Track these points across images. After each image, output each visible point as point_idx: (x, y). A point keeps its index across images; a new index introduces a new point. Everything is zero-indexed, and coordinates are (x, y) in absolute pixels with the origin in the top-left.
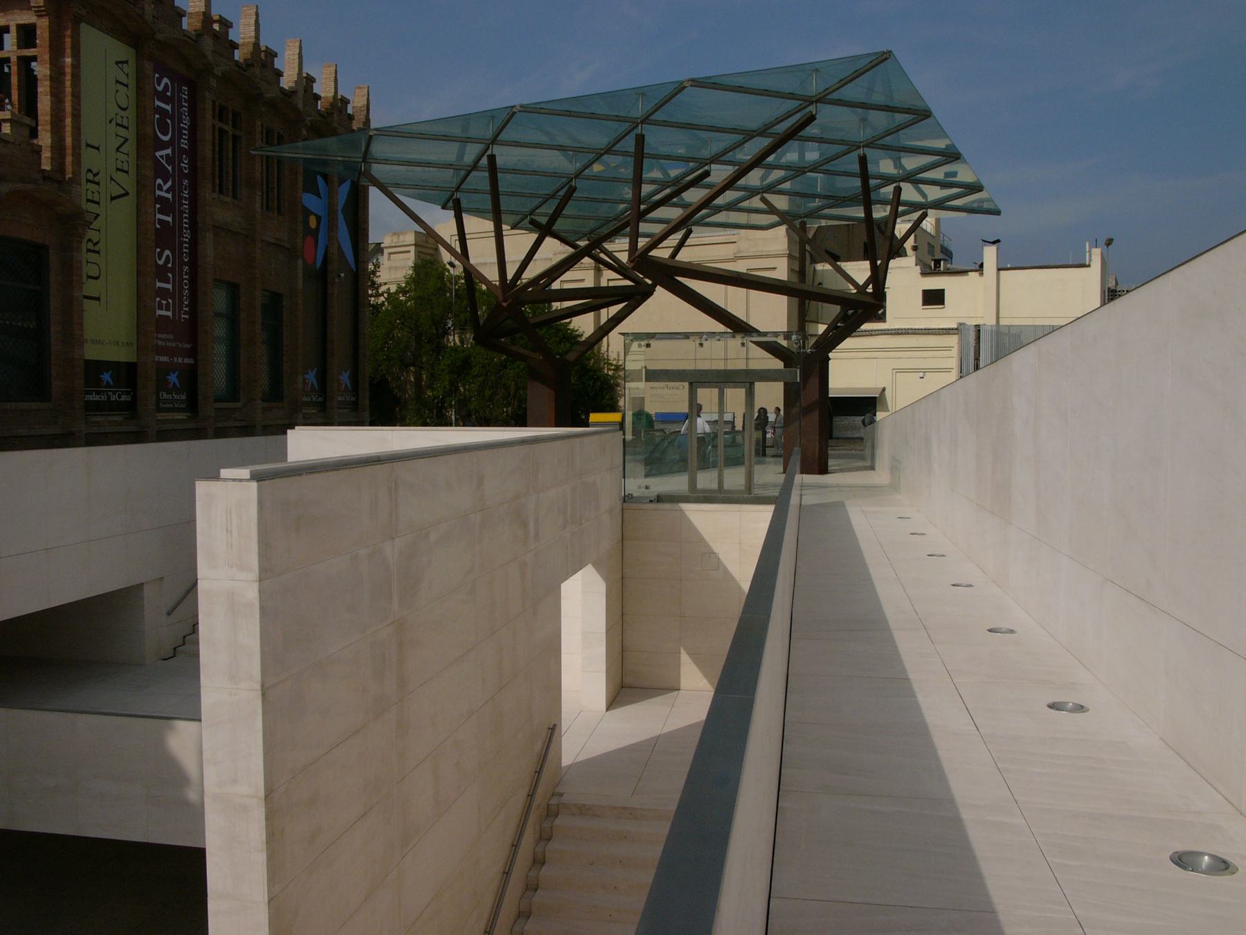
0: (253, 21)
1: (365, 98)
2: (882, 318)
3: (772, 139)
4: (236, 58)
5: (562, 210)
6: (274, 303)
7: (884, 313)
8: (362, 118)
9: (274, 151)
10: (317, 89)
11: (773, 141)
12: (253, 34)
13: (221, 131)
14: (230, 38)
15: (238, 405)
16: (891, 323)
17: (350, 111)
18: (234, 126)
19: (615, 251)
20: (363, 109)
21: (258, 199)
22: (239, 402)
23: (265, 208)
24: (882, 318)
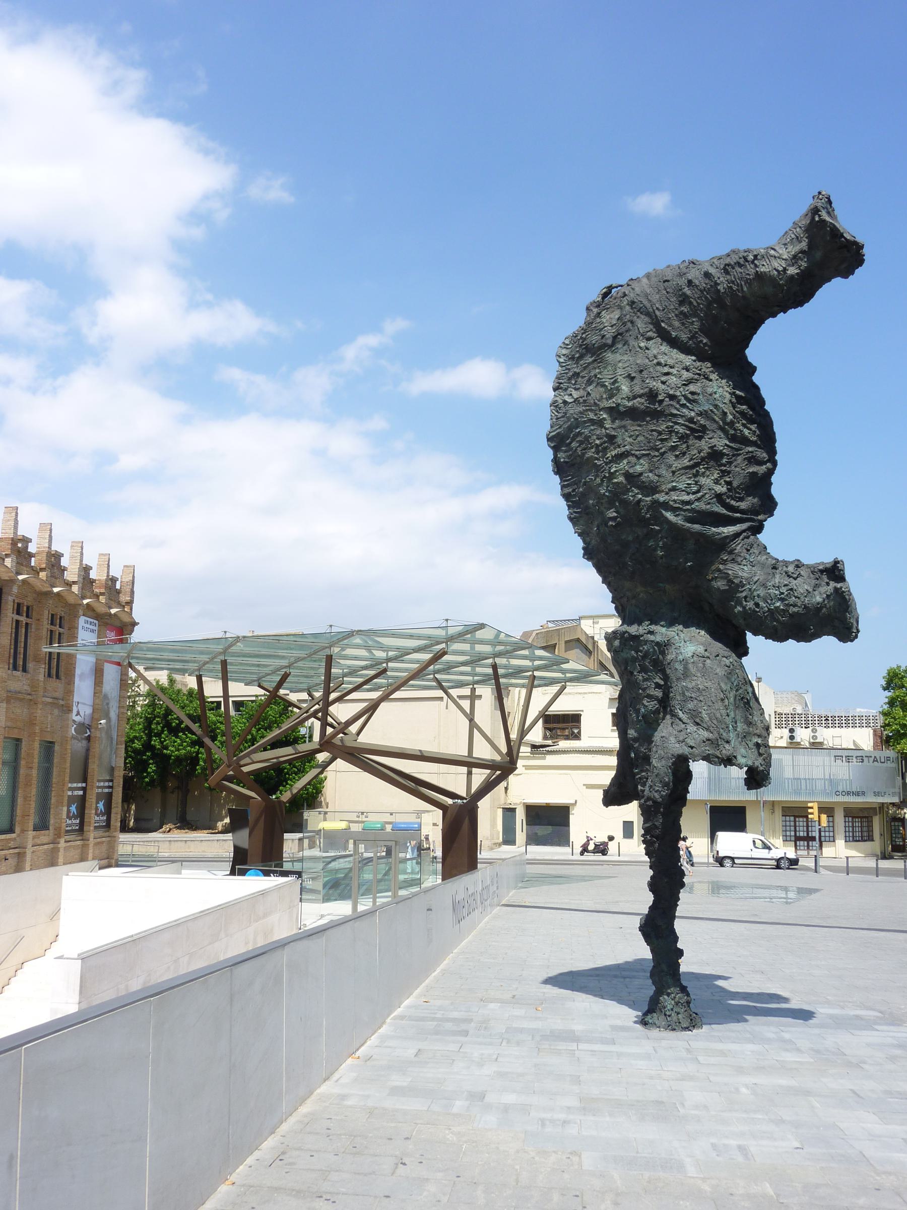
0: (47, 536)
1: (131, 575)
2: (577, 737)
3: (541, 719)
4: (33, 564)
5: (286, 679)
6: (48, 748)
7: (579, 733)
8: (128, 589)
9: (55, 648)
10: (93, 575)
11: (543, 720)
12: (47, 545)
13: (17, 622)
14: (29, 551)
15: (13, 836)
16: (584, 742)
17: (118, 587)
18: (27, 616)
19: (330, 716)
20: (129, 584)
21: (42, 670)
22: (14, 833)
23: (46, 676)
24: (577, 737)
